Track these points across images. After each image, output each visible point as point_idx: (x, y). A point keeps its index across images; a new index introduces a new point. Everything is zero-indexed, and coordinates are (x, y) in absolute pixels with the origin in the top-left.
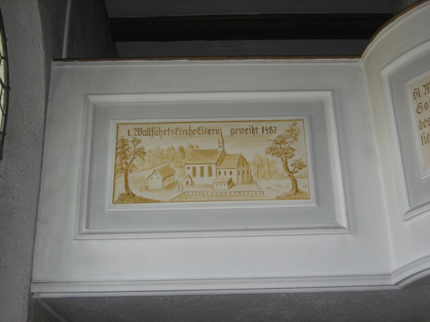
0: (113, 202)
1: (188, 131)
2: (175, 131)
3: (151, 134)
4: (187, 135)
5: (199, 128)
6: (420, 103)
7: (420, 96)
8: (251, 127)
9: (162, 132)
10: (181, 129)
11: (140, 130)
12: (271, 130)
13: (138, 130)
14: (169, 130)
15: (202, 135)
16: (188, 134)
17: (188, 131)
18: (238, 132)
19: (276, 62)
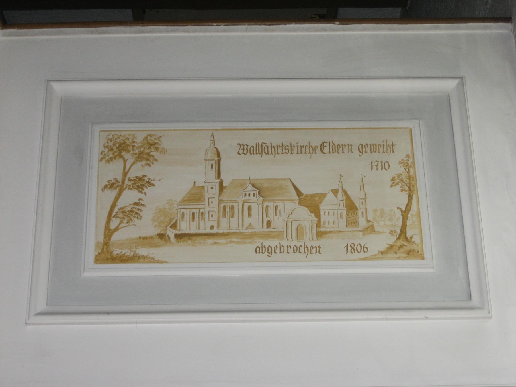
0: (411, 129)
1: (307, 148)
2: (290, 148)
3: (261, 152)
4: (306, 153)
5: (323, 143)
6: (360, 155)
7: (393, 152)
8: (385, 143)
9: (313, 148)
10: (299, 145)
11: (245, 147)
12: (353, 248)
13: (242, 147)
14: (282, 146)
15: (328, 154)
16: (308, 151)
17: (307, 148)
18: (368, 149)
19: (58, 34)
